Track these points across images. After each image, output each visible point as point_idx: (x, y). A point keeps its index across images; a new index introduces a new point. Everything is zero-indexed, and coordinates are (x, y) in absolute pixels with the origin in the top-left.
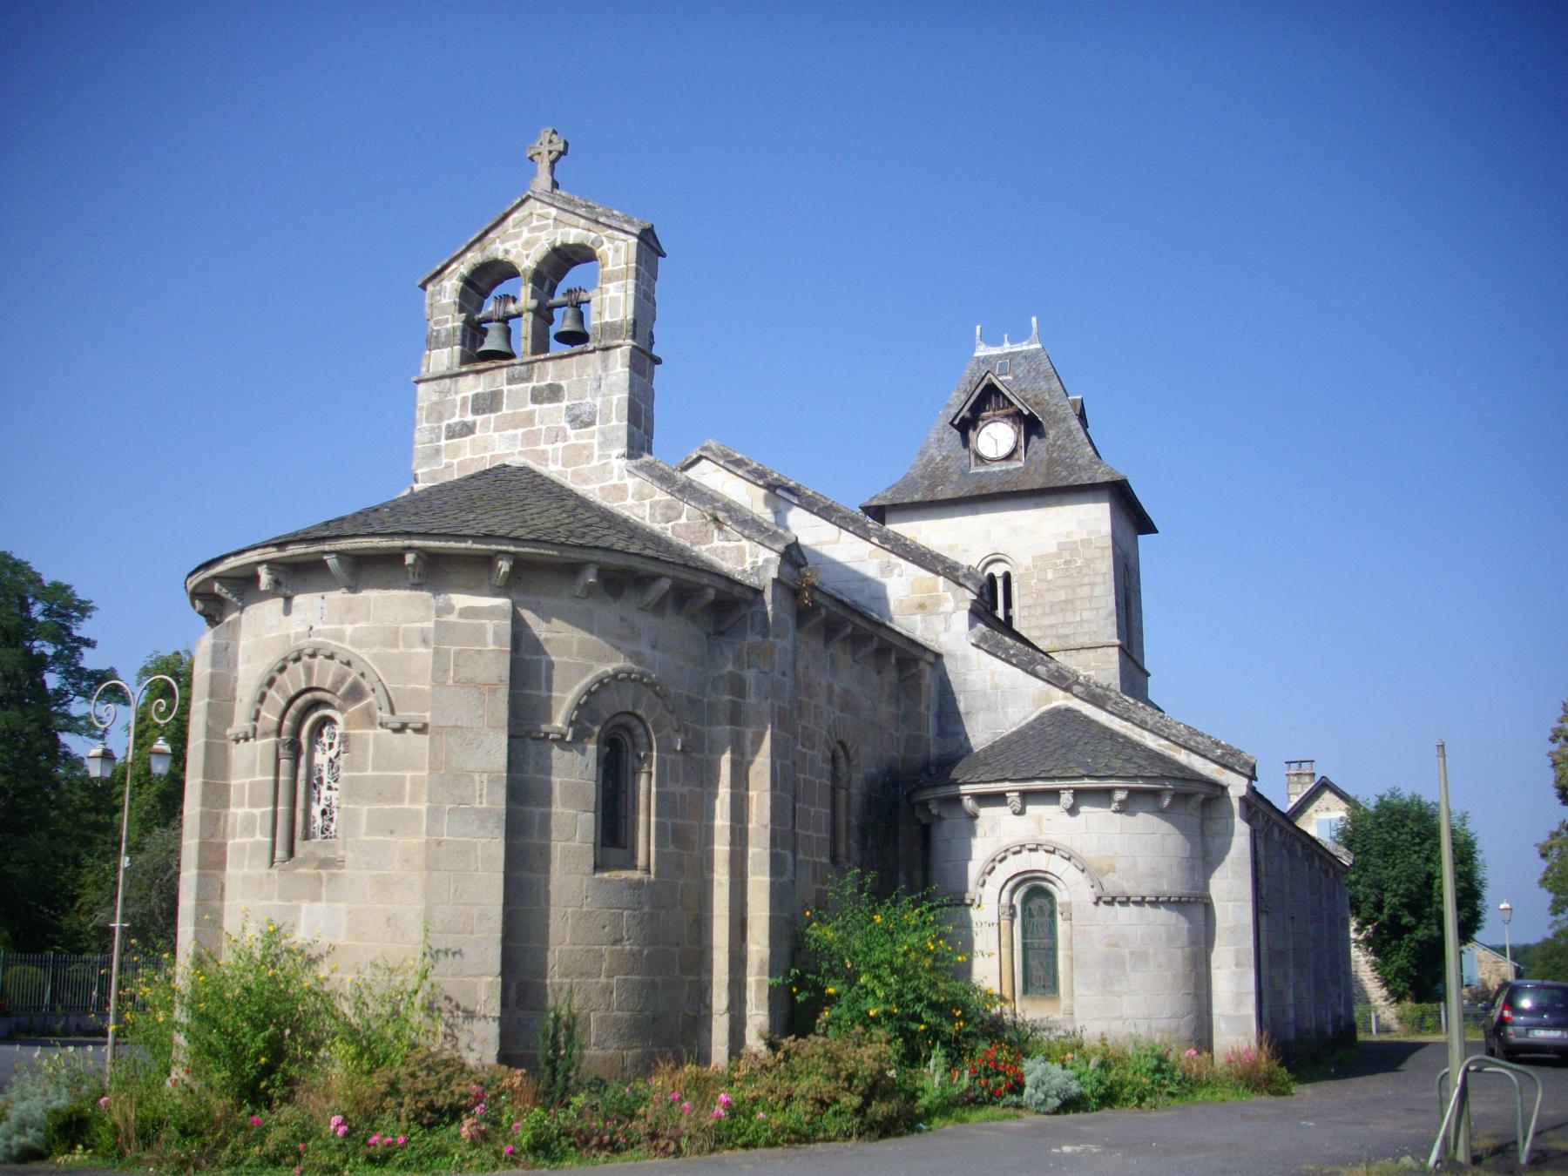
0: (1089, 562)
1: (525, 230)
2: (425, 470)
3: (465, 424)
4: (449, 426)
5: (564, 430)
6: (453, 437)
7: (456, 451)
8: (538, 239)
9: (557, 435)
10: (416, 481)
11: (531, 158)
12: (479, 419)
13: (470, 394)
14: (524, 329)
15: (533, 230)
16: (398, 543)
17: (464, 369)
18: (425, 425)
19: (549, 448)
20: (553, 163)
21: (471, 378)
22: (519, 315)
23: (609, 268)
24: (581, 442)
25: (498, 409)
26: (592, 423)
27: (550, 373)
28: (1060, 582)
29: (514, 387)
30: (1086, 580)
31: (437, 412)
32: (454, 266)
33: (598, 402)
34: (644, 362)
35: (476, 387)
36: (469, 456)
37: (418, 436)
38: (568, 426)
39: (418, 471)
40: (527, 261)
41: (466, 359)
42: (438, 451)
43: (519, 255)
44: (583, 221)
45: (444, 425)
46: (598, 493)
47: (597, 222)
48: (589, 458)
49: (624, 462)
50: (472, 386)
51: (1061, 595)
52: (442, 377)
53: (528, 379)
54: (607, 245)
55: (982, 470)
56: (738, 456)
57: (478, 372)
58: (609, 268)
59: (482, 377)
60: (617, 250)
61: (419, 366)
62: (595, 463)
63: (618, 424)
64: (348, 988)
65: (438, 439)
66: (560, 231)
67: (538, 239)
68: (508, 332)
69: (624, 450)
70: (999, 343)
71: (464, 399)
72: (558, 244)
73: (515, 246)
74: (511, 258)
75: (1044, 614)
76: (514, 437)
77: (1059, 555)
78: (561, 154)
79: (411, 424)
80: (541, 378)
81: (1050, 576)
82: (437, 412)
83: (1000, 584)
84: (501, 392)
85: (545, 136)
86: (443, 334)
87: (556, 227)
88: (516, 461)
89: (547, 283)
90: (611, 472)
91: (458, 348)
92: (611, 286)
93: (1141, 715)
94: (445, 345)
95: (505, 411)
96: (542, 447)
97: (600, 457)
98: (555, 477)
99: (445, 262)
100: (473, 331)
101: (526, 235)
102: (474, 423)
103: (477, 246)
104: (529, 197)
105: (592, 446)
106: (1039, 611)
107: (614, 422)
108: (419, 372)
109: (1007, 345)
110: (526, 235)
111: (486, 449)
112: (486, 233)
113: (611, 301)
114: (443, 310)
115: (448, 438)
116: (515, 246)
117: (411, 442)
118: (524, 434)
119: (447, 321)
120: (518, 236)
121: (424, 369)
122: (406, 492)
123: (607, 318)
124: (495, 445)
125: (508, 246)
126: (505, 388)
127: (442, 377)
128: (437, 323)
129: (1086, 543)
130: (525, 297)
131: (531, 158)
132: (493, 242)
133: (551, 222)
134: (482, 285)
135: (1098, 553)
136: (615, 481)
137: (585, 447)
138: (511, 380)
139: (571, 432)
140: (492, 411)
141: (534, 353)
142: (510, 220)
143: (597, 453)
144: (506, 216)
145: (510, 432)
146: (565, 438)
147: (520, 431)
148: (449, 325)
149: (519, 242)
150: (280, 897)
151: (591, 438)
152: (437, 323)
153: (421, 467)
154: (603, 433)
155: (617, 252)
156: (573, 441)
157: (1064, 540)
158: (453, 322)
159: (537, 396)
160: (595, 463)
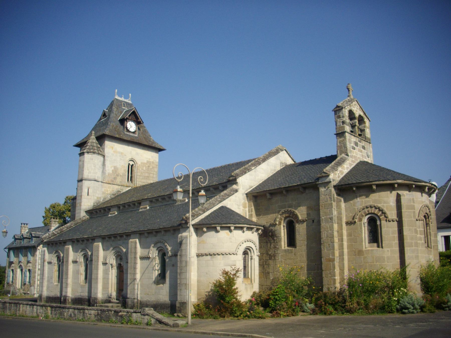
16: (412, 183)
30: (152, 172)
51: (147, 175)
55: (128, 133)
56: (434, 183)
64: (347, 304)
70: (121, 97)
75: (142, 179)
81: (144, 169)
83: (130, 167)
93: (429, 231)
106: (141, 177)
109: (123, 98)
129: (153, 162)
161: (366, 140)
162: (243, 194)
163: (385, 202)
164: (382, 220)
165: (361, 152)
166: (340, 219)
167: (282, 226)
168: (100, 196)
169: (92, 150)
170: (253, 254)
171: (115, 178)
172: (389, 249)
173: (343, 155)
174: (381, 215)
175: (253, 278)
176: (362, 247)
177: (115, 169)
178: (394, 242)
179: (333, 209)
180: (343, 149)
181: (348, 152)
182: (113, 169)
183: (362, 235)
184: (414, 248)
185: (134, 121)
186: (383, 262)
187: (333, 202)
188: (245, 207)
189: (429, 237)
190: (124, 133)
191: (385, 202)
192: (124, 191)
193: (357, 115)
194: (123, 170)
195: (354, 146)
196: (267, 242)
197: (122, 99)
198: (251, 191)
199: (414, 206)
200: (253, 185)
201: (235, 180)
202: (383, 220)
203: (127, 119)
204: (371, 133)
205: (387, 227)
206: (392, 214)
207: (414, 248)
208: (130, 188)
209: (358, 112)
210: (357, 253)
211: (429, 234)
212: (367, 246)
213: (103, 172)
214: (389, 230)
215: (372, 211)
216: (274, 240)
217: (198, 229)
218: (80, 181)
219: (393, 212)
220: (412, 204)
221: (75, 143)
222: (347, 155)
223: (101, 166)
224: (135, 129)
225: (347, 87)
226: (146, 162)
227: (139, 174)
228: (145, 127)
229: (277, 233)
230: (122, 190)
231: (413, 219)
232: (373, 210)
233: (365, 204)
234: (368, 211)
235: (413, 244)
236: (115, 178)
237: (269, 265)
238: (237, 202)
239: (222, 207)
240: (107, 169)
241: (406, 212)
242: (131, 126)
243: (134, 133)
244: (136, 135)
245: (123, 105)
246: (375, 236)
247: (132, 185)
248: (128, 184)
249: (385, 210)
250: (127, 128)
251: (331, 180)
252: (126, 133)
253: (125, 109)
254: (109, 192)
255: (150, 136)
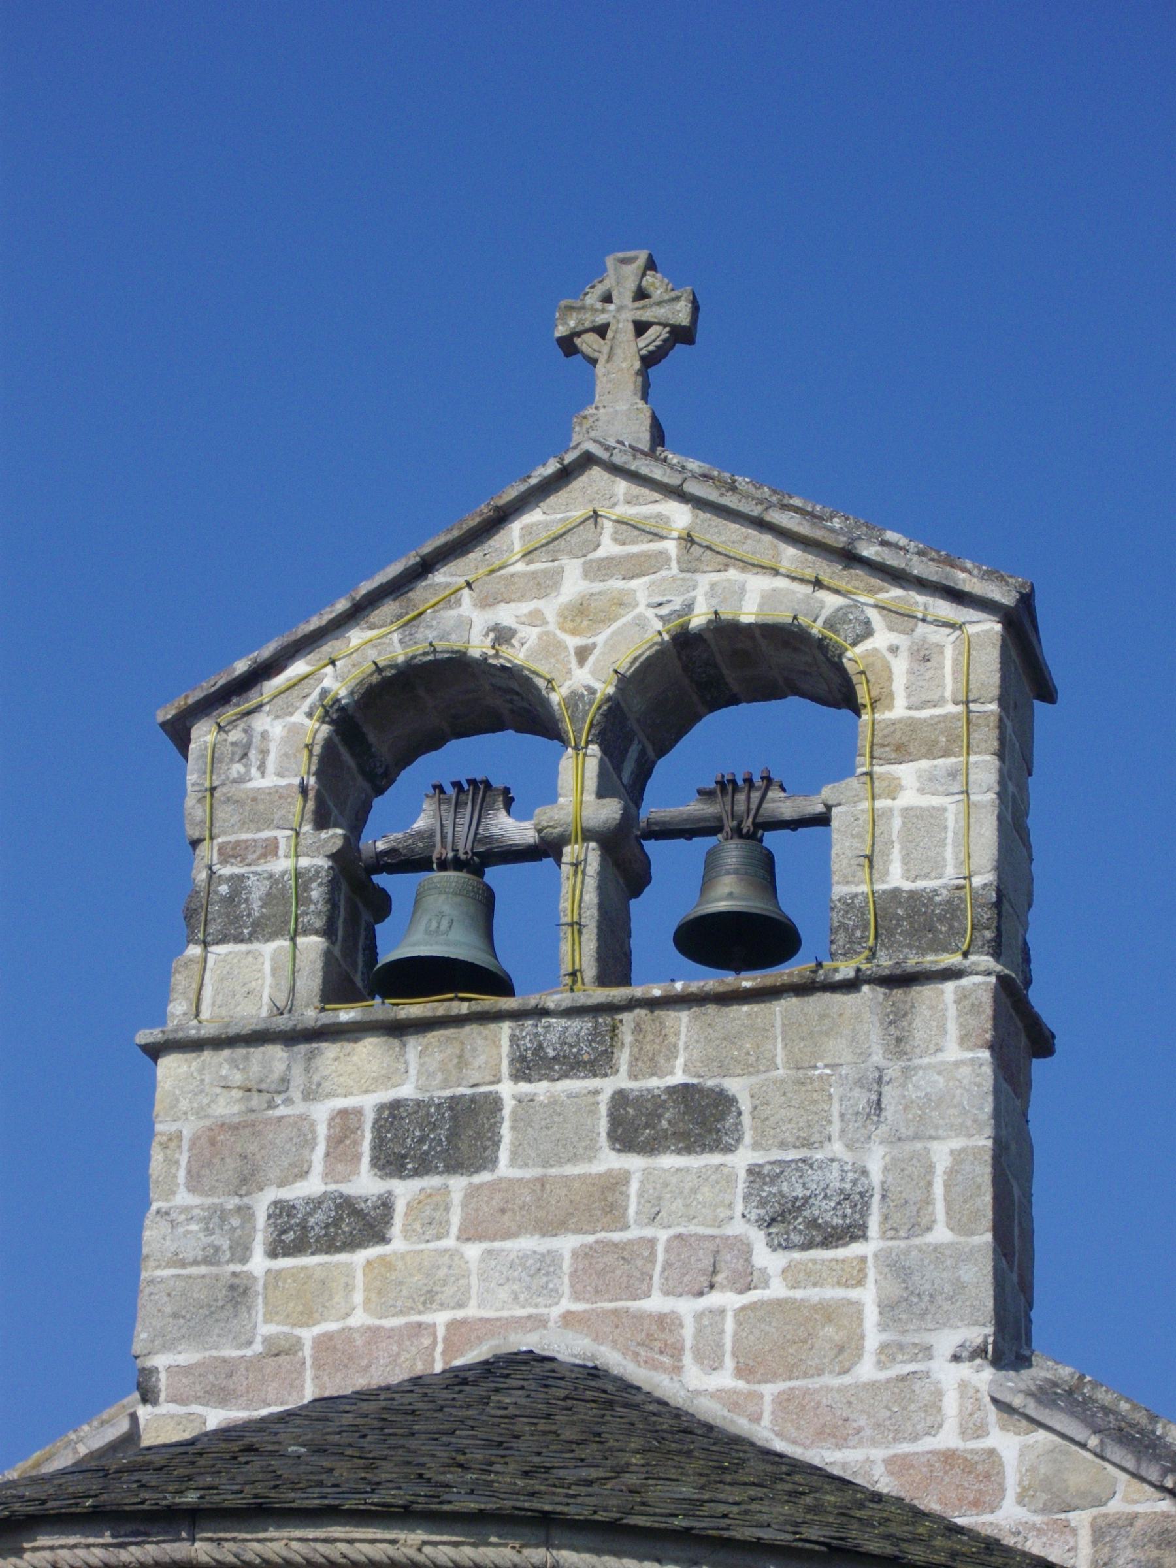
1: (572, 568)
2: (186, 1357)
3: (347, 1206)
4: (282, 1209)
5: (745, 1250)
6: (298, 1248)
7: (311, 1301)
8: (622, 602)
9: (713, 1265)
10: (148, 1396)
11: (568, 345)
12: (404, 1191)
13: (369, 1102)
15: (600, 570)
17: (347, 1014)
18: (183, 1198)
19: (686, 1307)
20: (649, 361)
21: (369, 1049)
22: (547, 849)
23: (899, 710)
24: (813, 1294)
25: (483, 1159)
26: (854, 1232)
27: (683, 1051)
29: (541, 1089)
31: (234, 1156)
32: (299, 668)
33: (876, 1162)
34: (1020, 1036)
35: (387, 1079)
36: (359, 1319)
37: (153, 1235)
38: (758, 1237)
39: (160, 1361)
40: (582, 671)
41: (337, 988)
42: (238, 1293)
43: (550, 647)
44: (790, 554)
45: (262, 1203)
46: (878, 1471)
47: (849, 558)
48: (847, 1351)
49: (984, 1376)
50: (369, 1076)
52: (259, 1038)
53: (599, 1063)
54: (882, 639)
57: (398, 1029)
58: (899, 710)
59: (414, 1045)
60: (924, 656)
61: (163, 996)
62: (867, 1370)
63: (958, 1239)
65: (242, 1252)
66: (704, 581)
67: (622, 602)
68: (486, 902)
69: (981, 1332)
71: (346, 1121)
72: (698, 620)
73: (536, 619)
74: (517, 655)
76: (546, 1264)
78: (681, 335)
79: (132, 1195)
80: (648, 1063)
82: (234, 1156)
84: (494, 1104)
85: (621, 276)
86: (257, 891)
87: (690, 567)
88: (570, 1347)
89: (633, 752)
90: (934, 1405)
91: (313, 945)
92: (906, 772)
94: (261, 930)
95: (505, 1168)
96: (656, 1303)
97: (888, 1354)
98: (711, 1410)
99: (267, 651)
100: (357, 894)
101: (574, 584)
102: (386, 1205)
103: (389, 608)
104: (587, 461)
105: (857, 1308)
107: (941, 1234)
108: (160, 1018)
110: (574, 584)
111: (429, 1299)
112: (426, 567)
113: (913, 816)
114: (258, 810)
115: (273, 1254)
116: (536, 619)
117: (131, 1256)
118: (584, 1255)
119: (270, 849)
120: (546, 584)
121: (178, 1008)
122: (92, 1438)
123: (896, 877)
124: (451, 1287)
125: (506, 615)
126: (507, 1090)
127: (259, 1038)
128: (229, 854)
130: (575, 793)
131: (568, 345)
132: (450, 599)
133: (671, 547)
134: (381, 743)
136: (948, 1438)
137: (827, 1312)
138: (528, 1065)
139: (765, 1258)
140: (455, 1166)
141: (603, 980)
142: (515, 528)
143: (873, 1339)
144: (501, 518)
145: (528, 1243)
146: (746, 1280)
147: (567, 1244)
148: (282, 865)
149: (550, 607)
151: (858, 1283)
152: (229, 854)
153: (168, 1346)
154: (896, 1267)
155: (924, 662)
156: (777, 1289)
158: (300, 854)
159: (634, 1126)
160: (867, 1370)
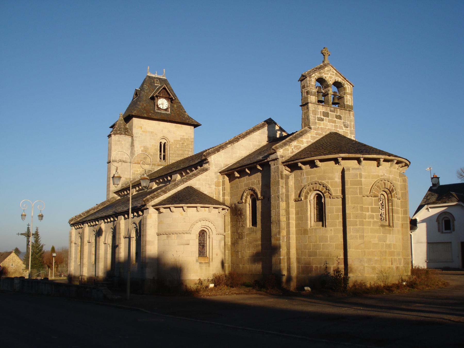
0: (188, 145)
7: (320, 124)
12: (325, 118)
14: (331, 98)
26: (348, 127)
28: (180, 148)
30: (187, 149)
51: (181, 152)
75: (176, 157)
77: (180, 141)
81: (178, 146)
101: (329, 75)
106: (174, 155)
110: (329, 75)
125: (326, 76)
135: (190, 143)
150: (383, 233)
157: (182, 137)
161: (350, 108)
162: (216, 173)
163: (330, 178)
164: (326, 197)
165: (335, 122)
166: (287, 197)
167: (248, 205)
168: (128, 177)
169: (118, 132)
170: (211, 233)
171: (145, 158)
172: (332, 228)
173: (306, 128)
174: (325, 192)
175: (211, 257)
176: (307, 226)
177: (146, 149)
178: (338, 221)
179: (280, 187)
180: (306, 122)
181: (311, 125)
182: (142, 149)
183: (307, 213)
184: (358, 227)
185: (165, 98)
186: (326, 242)
187: (280, 179)
188: (217, 185)
189: (391, 214)
190: (154, 111)
191: (330, 178)
192: (156, 170)
193: (331, 82)
194: (154, 148)
195: (322, 117)
196: (237, 221)
197: (156, 75)
198: (227, 168)
199: (361, 181)
200: (229, 163)
201: (206, 159)
202: (327, 197)
203: (157, 96)
204: (354, 100)
205: (331, 205)
206: (336, 191)
207: (358, 227)
208: (162, 167)
209: (330, 76)
210: (302, 231)
211: (390, 211)
212: (312, 225)
213: (132, 153)
214: (333, 207)
215: (316, 187)
216: (242, 218)
217: (157, 207)
218: (109, 162)
219: (338, 189)
220: (359, 179)
221: (110, 126)
222: (310, 128)
223: (129, 147)
224: (167, 106)
225: (322, 51)
226: (179, 139)
227: (172, 152)
228: (180, 103)
229: (243, 211)
230: (154, 169)
231: (359, 195)
232: (321, 188)
233: (311, 180)
234: (319, 187)
235: (358, 223)
236: (145, 158)
237: (238, 243)
238: (207, 181)
239: (188, 187)
240: (136, 149)
241: (350, 188)
242: (163, 103)
243: (166, 110)
244: (169, 113)
245: (155, 82)
246: (321, 216)
247: (164, 164)
248: (160, 163)
249: (329, 186)
250: (157, 106)
251: (279, 157)
252: (156, 111)
253: (157, 86)
254: (139, 172)
255: (185, 112)
